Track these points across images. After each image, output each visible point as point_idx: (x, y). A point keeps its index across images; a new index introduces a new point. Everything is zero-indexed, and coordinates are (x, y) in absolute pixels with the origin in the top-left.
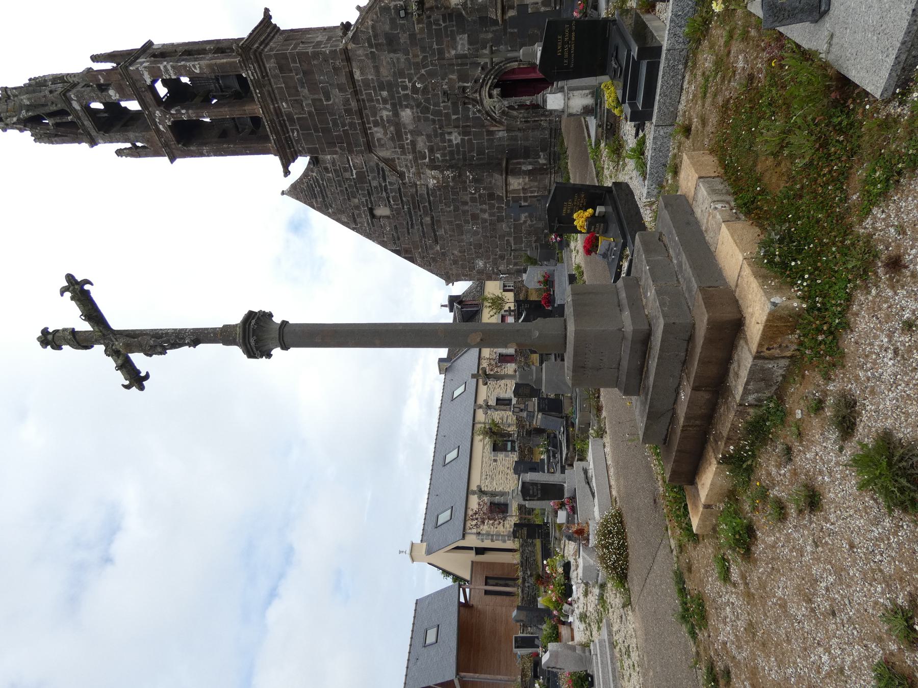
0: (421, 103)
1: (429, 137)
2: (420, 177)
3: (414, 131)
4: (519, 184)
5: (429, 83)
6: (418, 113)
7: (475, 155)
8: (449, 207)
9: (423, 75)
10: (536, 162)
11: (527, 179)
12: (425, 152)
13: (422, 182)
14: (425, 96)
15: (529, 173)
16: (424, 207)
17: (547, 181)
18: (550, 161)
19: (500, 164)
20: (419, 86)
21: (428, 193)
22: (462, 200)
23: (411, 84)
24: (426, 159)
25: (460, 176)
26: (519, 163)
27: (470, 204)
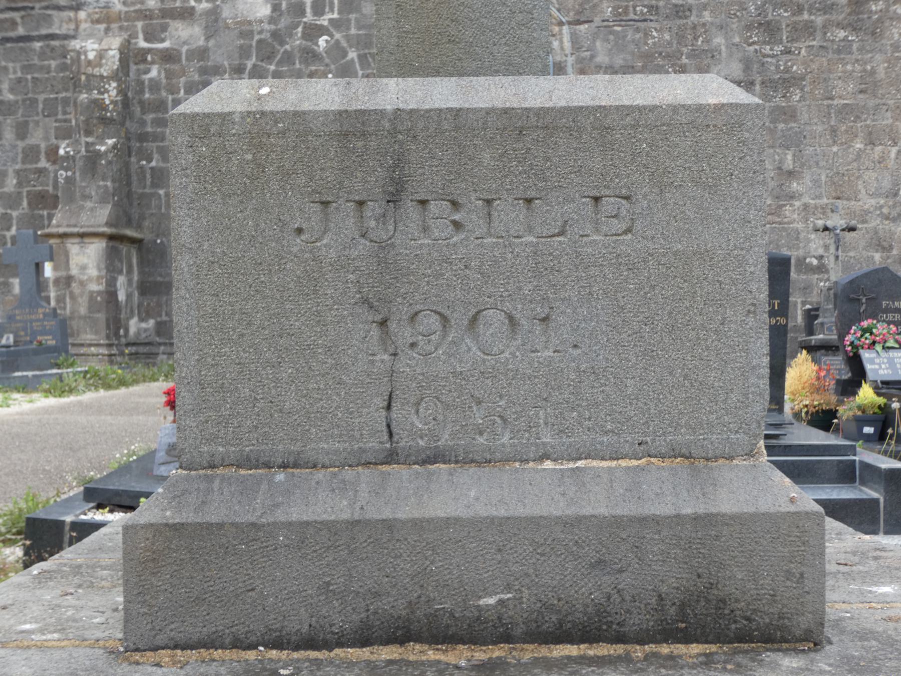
0: (282, 43)
1: (202, 53)
2: (98, 21)
3: (216, 21)
4: (83, 268)
5: (327, 65)
6: (260, 33)
7: (153, 164)
8: (11, 90)
9: (345, 54)
10: (132, 311)
11: (94, 287)
12: (163, 40)
13: (83, 26)
14: (298, 55)
15: (111, 294)
16: (14, 23)
17: (89, 336)
18: (134, 344)
19: (129, 223)
20: (322, 41)
21: (52, 37)
22: (31, 125)
23: (326, 23)
24: (146, 40)
25: (104, 120)
26: (130, 271)
27: (21, 144)
